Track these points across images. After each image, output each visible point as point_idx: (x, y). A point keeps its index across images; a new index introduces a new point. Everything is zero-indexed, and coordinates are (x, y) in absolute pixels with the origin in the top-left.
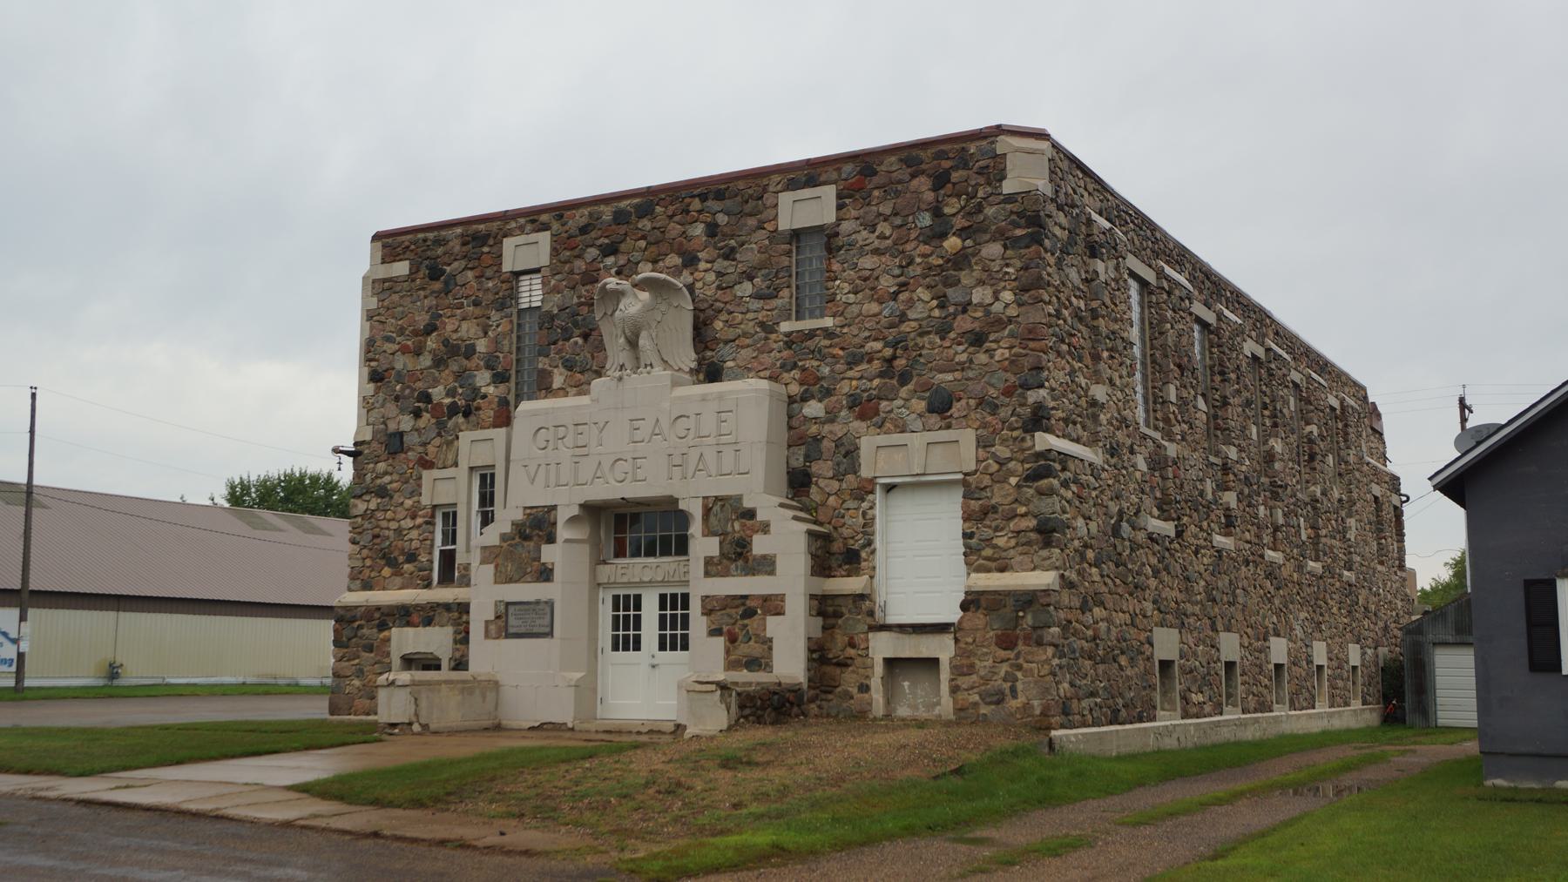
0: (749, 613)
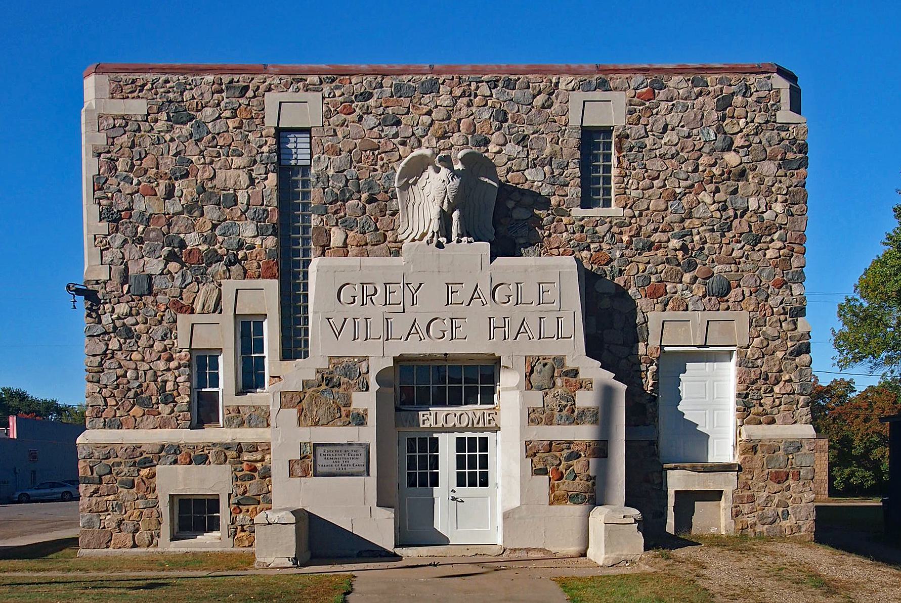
0: (147, 463)
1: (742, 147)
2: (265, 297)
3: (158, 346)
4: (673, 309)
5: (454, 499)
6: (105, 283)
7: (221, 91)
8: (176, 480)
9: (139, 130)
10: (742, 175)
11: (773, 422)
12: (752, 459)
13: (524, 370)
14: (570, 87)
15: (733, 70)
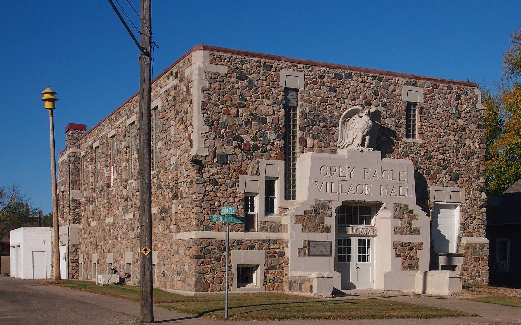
0: (411, 249)
1: (464, 117)
2: (277, 169)
3: (230, 190)
4: (439, 186)
5: (357, 268)
6: (205, 157)
7: (260, 66)
8: (240, 257)
9: (223, 81)
10: (464, 130)
11: (472, 236)
12: (468, 252)
13: (393, 209)
14: (403, 83)
15: (462, 84)
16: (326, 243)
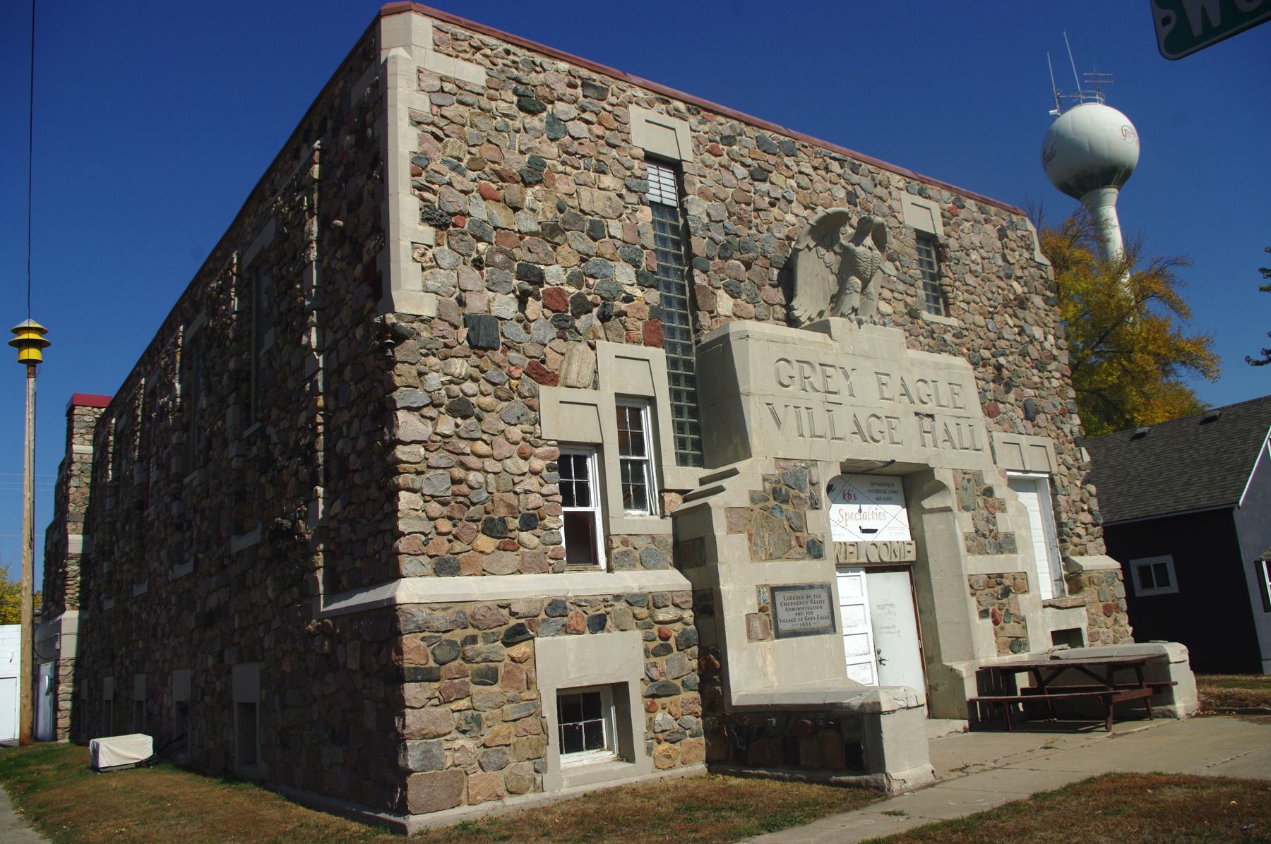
0: (516, 635)
8: (566, 661)
16: (813, 592)
